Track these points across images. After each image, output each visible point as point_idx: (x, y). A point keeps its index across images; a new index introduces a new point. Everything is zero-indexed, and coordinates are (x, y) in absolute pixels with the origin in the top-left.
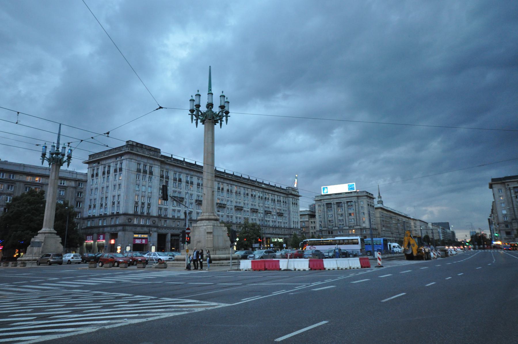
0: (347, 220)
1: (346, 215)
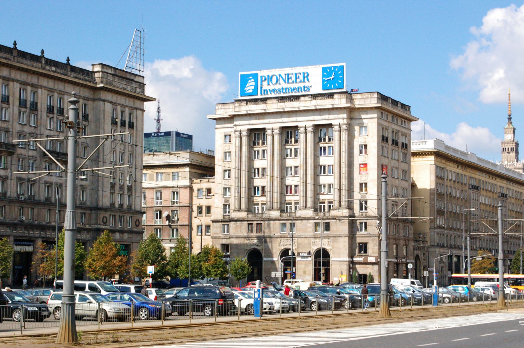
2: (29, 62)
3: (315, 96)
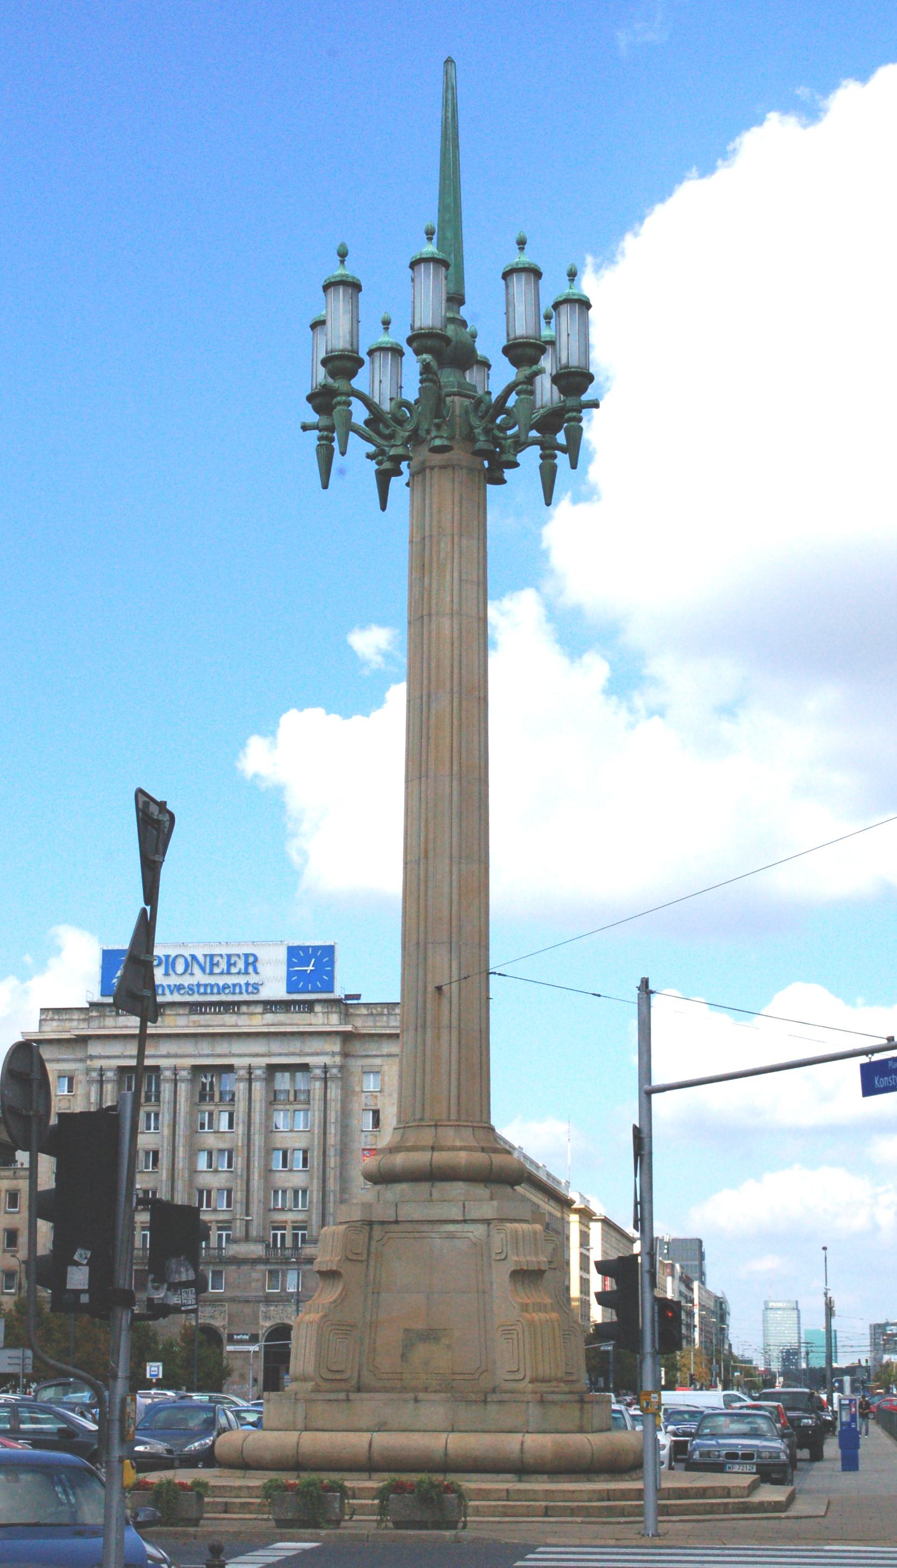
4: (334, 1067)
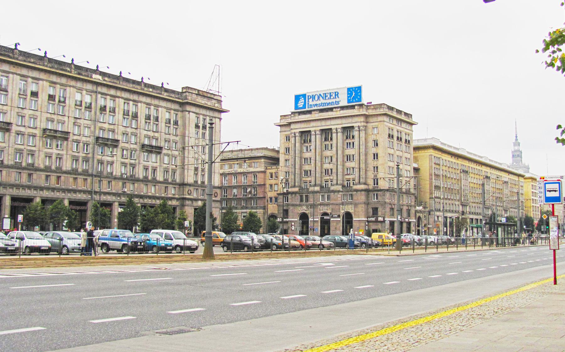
0: (340, 170)
1: (340, 160)
2: (131, 85)
3: (343, 108)
4: (362, 126)
